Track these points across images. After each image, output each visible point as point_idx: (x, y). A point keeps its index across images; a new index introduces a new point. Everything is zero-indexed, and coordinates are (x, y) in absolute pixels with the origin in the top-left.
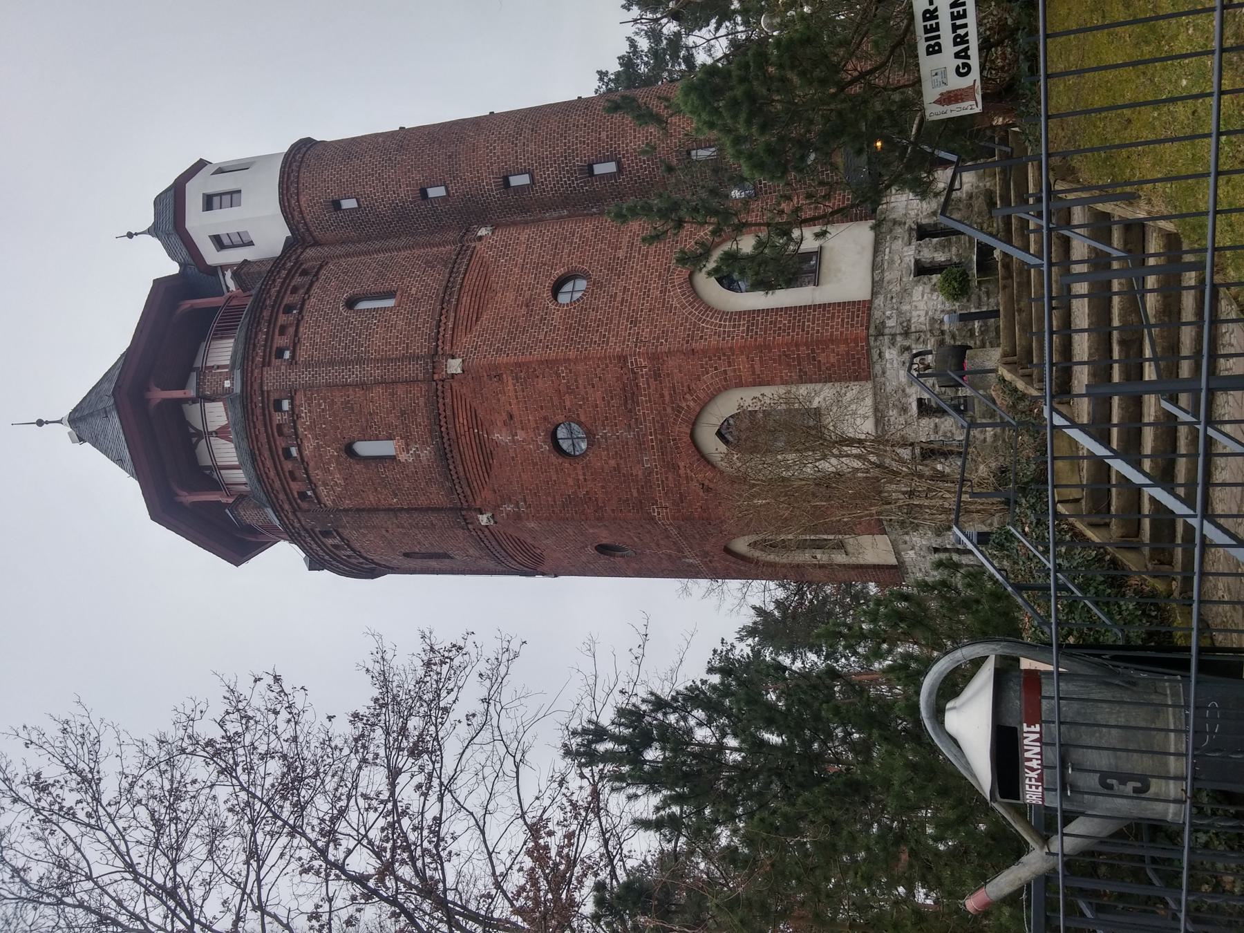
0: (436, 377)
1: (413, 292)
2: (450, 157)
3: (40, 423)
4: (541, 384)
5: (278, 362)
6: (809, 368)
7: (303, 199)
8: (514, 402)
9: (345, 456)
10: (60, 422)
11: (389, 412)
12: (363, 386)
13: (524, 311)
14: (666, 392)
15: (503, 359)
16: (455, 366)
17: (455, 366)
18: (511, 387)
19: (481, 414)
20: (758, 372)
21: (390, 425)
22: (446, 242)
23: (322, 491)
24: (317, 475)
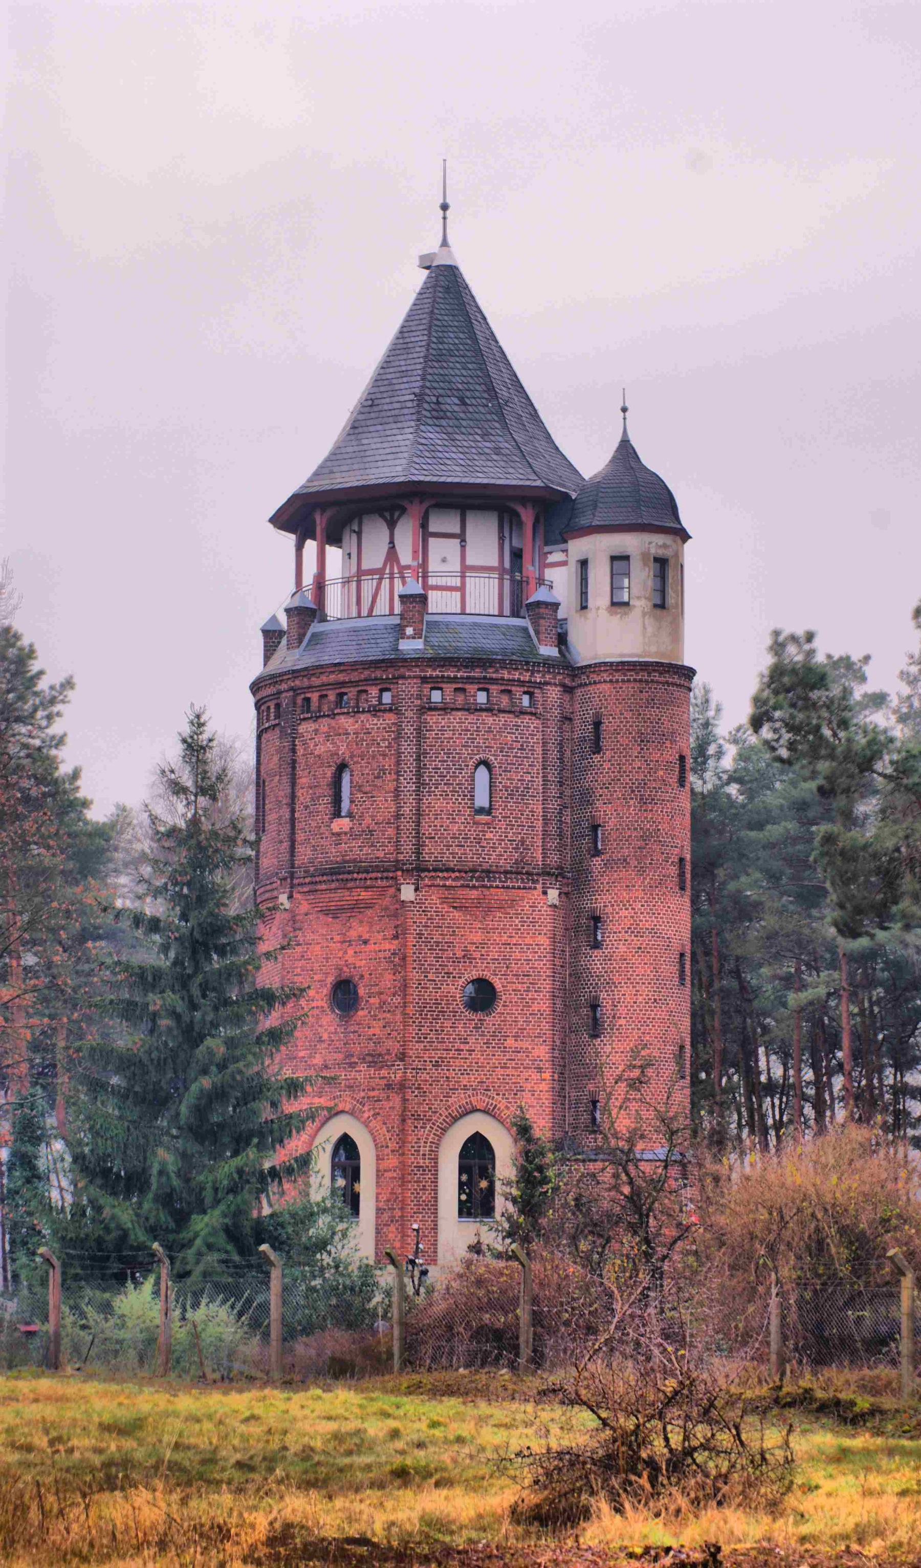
0: (399, 873)
2: (625, 860)
3: (445, 207)
5: (426, 691)
6: (386, 1216)
7: (606, 687)
8: (377, 947)
9: (339, 762)
10: (445, 243)
11: (373, 817)
12: (397, 792)
13: (460, 954)
14: (376, 1093)
15: (411, 939)
16: (407, 893)
17: (407, 893)
18: (387, 946)
19: (369, 912)
20: (386, 1174)
22: (545, 856)
24: (324, 725)
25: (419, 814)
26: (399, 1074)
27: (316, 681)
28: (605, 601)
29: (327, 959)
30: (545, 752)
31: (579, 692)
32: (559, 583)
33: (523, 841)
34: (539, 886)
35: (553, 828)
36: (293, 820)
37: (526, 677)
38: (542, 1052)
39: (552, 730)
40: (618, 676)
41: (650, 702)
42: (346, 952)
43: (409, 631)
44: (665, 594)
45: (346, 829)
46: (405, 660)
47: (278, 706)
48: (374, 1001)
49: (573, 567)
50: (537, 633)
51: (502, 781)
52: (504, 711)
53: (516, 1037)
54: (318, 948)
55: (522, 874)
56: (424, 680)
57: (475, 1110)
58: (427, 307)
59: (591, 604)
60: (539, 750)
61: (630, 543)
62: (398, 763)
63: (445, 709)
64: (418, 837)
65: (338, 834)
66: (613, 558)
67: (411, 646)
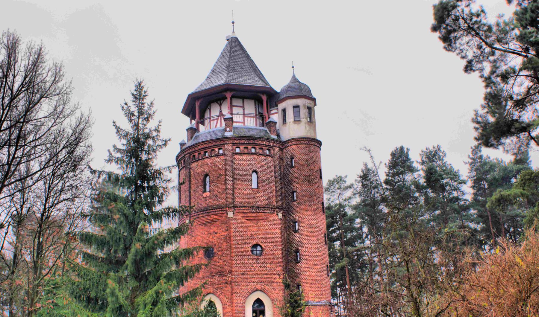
1: (258, 195)
4: (225, 244)
5: (234, 148)
7: (294, 146)
8: (220, 234)
10: (233, 32)
11: (217, 191)
12: (225, 182)
13: (249, 235)
14: (221, 285)
15: (232, 231)
16: (230, 214)
17: (230, 214)
18: (224, 234)
19: (217, 223)
21: (214, 191)
22: (277, 202)
23: (195, 164)
24: (200, 163)
25: (233, 188)
26: (230, 278)
27: (197, 149)
28: (292, 120)
29: (203, 240)
30: (275, 168)
31: (285, 150)
32: (276, 117)
33: (269, 197)
34: (275, 212)
35: (279, 194)
36: (190, 195)
37: (268, 143)
38: (280, 269)
39: (277, 162)
40: (298, 143)
41: (309, 151)
42: (209, 237)
43: (228, 129)
44: (311, 121)
45: (208, 195)
46: (227, 138)
47: (184, 160)
48: (220, 253)
49: (280, 112)
50: (270, 131)
51: (261, 177)
52: (261, 155)
53: (270, 264)
54: (200, 237)
55: (270, 208)
56: (234, 144)
57: (257, 290)
58: (229, 46)
59: (287, 121)
60: (273, 168)
61: (299, 102)
62: (226, 172)
63: (240, 154)
64: (233, 196)
65: (206, 198)
66: (294, 107)
67: (228, 134)
